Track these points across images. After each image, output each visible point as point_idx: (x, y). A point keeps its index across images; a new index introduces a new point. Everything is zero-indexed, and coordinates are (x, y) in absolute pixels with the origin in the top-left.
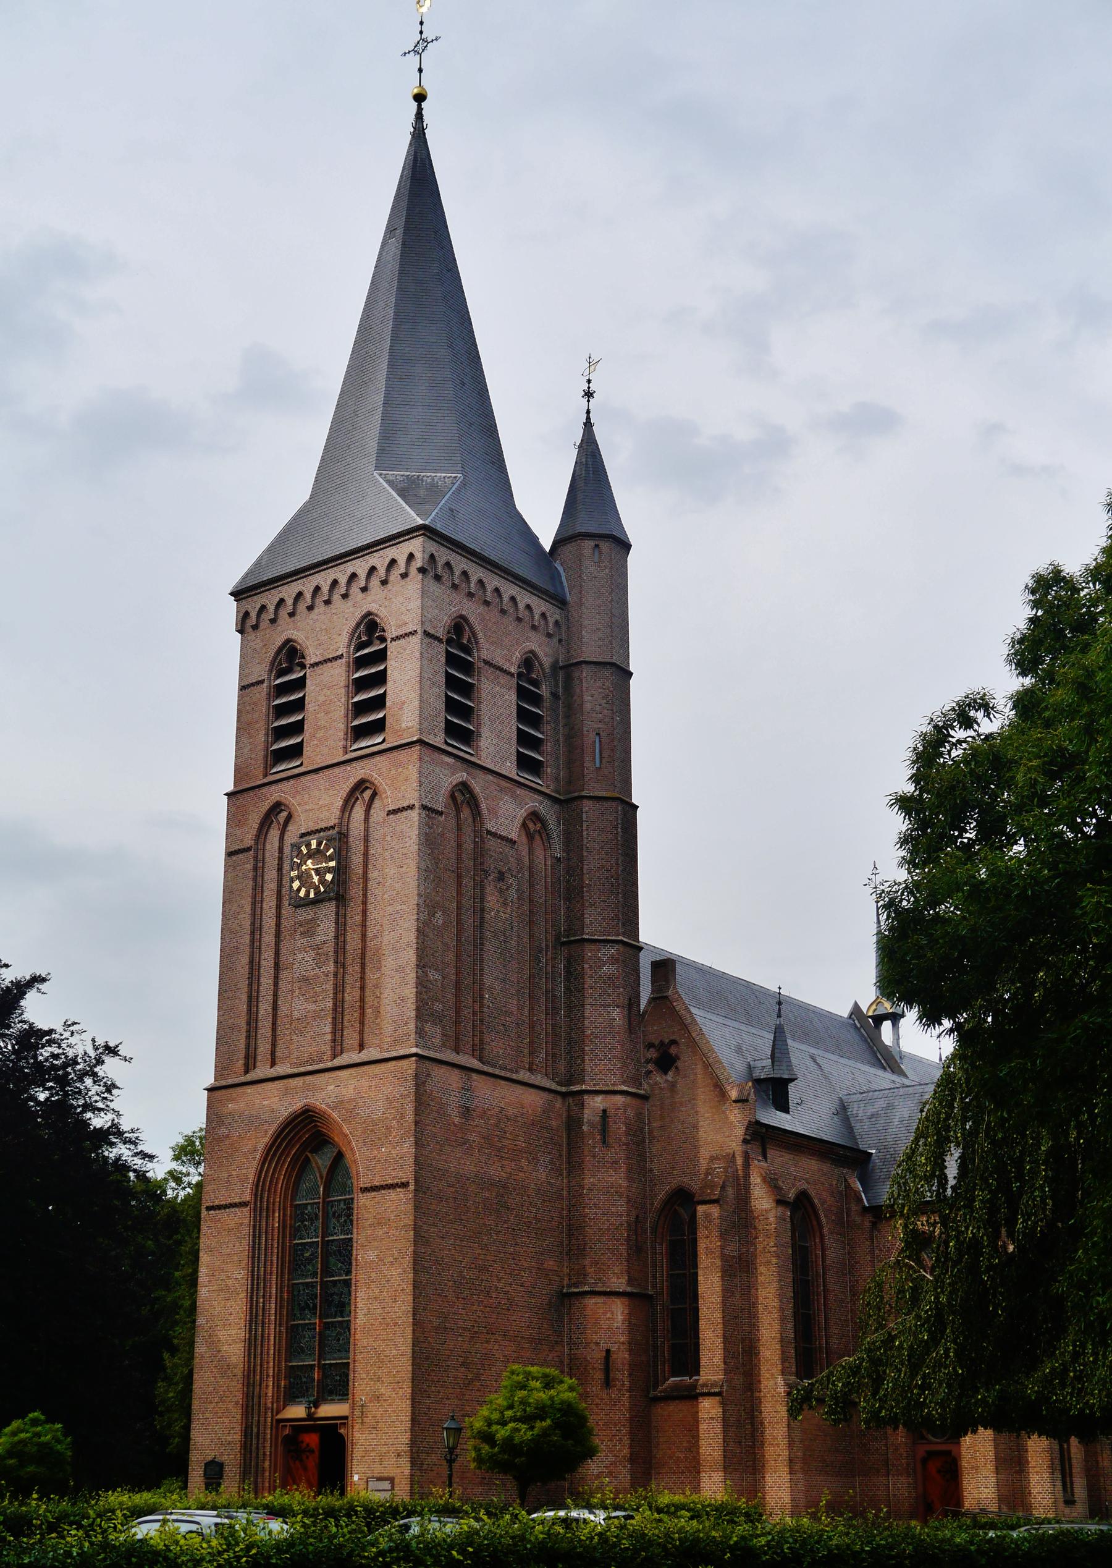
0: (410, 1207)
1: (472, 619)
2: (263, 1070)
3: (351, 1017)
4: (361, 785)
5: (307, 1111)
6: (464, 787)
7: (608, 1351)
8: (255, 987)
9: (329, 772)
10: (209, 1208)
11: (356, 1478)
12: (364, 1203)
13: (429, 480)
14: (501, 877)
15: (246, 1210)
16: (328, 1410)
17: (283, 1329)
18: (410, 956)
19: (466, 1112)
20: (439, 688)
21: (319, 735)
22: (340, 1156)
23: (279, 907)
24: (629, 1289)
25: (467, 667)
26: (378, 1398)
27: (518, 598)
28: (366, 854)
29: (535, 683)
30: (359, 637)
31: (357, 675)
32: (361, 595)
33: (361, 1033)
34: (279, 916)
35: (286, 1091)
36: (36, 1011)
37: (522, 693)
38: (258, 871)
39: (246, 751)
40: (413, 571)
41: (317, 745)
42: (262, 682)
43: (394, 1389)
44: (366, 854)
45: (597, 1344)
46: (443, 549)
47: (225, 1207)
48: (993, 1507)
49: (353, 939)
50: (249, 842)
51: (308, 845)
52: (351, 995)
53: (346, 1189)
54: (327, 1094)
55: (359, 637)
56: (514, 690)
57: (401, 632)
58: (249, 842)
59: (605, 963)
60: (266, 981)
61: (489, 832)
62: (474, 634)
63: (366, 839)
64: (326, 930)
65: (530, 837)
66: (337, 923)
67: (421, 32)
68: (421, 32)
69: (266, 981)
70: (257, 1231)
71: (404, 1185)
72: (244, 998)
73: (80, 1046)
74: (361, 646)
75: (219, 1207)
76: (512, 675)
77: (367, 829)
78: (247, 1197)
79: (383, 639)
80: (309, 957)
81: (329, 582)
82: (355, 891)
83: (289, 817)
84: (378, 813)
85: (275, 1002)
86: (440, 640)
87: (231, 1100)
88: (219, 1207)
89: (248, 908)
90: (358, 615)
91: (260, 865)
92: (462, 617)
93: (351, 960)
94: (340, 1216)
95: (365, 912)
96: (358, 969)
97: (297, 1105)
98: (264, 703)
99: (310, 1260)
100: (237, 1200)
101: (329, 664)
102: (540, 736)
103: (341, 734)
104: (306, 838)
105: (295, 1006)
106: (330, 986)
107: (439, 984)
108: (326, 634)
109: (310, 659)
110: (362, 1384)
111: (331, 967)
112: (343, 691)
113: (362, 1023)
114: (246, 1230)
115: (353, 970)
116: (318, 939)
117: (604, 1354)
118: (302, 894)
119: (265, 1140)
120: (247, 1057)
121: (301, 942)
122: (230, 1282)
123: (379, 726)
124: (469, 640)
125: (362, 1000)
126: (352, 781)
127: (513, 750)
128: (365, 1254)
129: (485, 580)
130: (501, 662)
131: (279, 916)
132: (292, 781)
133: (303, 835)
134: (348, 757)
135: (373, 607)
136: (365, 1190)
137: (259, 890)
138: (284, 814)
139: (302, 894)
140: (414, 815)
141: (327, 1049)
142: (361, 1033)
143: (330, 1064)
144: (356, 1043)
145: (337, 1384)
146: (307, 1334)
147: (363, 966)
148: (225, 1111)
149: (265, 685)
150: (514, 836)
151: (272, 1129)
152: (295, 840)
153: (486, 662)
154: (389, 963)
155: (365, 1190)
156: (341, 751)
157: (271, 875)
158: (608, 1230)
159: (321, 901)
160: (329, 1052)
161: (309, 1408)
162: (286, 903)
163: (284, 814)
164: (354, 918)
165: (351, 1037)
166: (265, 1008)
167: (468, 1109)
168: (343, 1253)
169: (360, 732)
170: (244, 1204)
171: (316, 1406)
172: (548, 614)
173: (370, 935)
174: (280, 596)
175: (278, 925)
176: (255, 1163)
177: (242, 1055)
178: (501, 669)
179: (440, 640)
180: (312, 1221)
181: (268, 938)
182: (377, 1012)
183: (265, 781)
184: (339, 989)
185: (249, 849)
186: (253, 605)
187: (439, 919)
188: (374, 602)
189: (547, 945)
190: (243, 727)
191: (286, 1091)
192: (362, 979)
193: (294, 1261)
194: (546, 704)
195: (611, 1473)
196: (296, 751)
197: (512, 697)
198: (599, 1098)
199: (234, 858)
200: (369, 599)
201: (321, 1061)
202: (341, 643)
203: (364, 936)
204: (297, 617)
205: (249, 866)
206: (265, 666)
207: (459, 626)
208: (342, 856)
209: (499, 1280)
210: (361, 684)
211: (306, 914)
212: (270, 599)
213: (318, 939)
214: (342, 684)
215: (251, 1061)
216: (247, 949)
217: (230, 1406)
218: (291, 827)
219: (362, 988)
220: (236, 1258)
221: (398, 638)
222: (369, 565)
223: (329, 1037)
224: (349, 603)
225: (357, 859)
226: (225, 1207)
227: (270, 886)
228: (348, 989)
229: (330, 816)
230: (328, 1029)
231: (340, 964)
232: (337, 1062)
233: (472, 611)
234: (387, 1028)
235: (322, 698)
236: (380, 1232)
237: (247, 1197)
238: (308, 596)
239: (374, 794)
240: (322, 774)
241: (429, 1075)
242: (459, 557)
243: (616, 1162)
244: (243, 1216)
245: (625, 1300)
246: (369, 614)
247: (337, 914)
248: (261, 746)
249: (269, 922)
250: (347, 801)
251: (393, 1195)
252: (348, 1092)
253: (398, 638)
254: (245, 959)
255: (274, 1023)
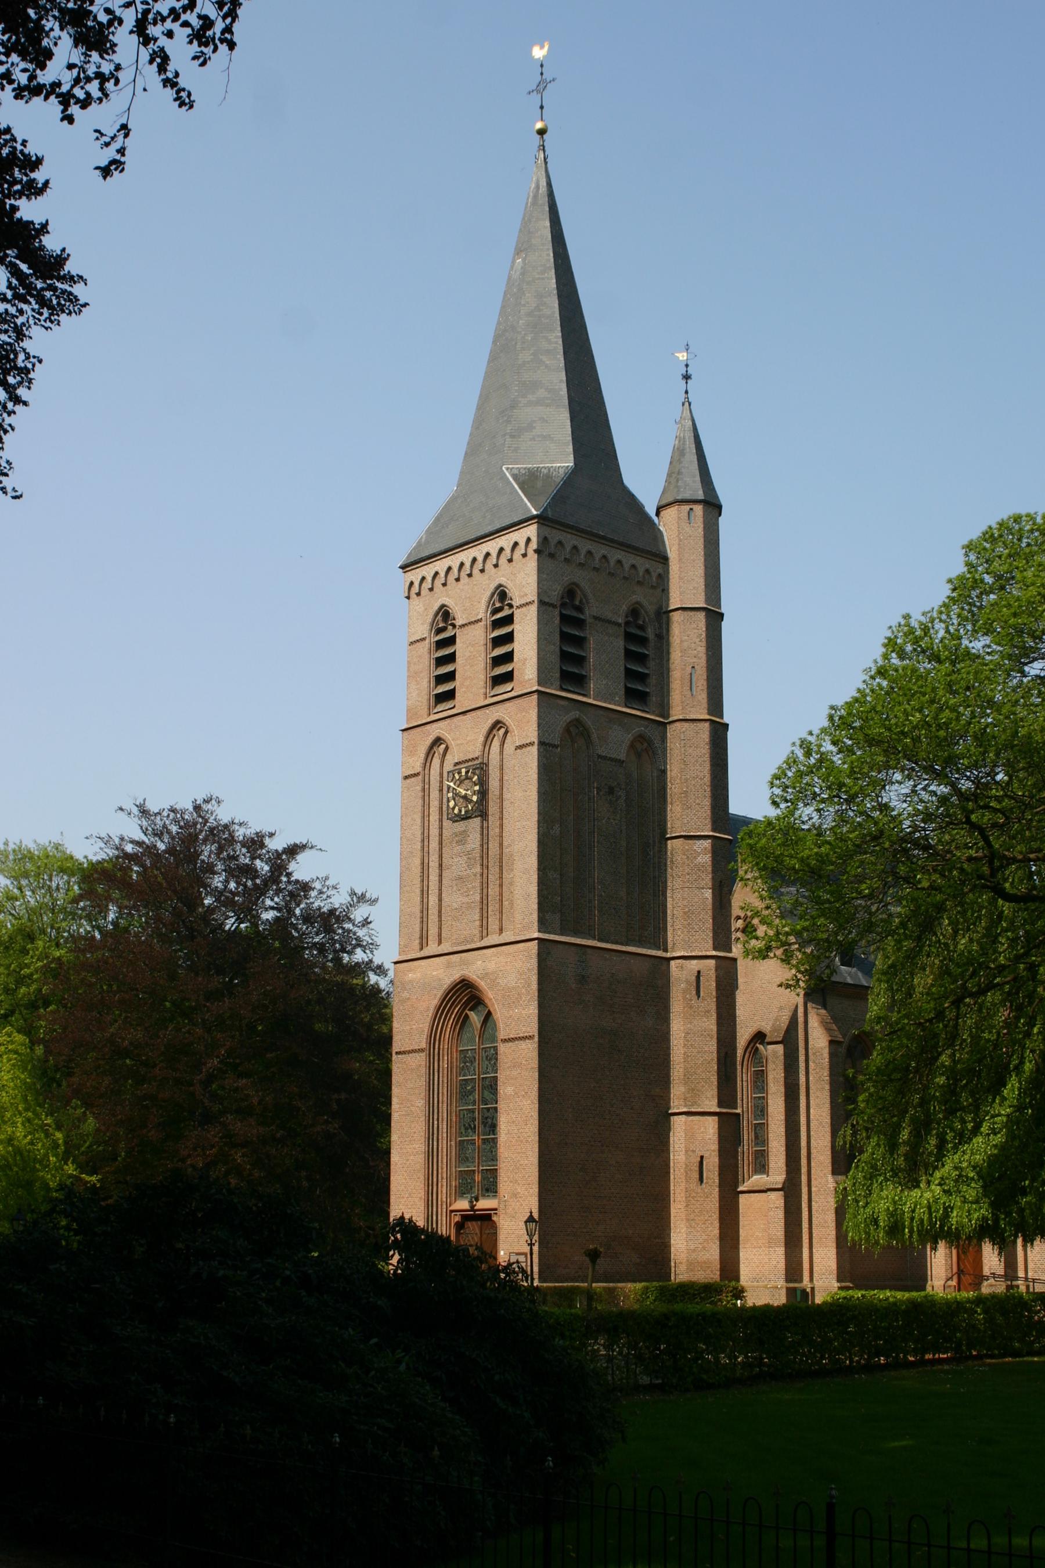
0: (535, 1054)
1: (582, 584)
2: (432, 948)
3: (493, 907)
4: (497, 724)
5: (463, 980)
6: (577, 723)
7: (702, 1157)
8: (425, 883)
9: (473, 714)
10: (397, 1053)
11: (502, 1253)
12: (504, 1050)
13: (546, 471)
14: (611, 791)
15: (423, 1055)
16: (483, 1204)
17: (453, 1143)
18: (533, 861)
19: (583, 979)
20: (554, 644)
21: (467, 683)
22: (489, 1014)
23: (441, 820)
24: (718, 1110)
25: (580, 623)
26: (515, 1195)
27: (624, 561)
28: (501, 780)
29: (642, 628)
30: (494, 604)
31: (493, 635)
32: (494, 570)
33: (501, 920)
34: (441, 828)
35: (449, 965)
36: (301, 869)
37: (629, 637)
38: (425, 792)
39: (414, 695)
40: (530, 552)
41: (465, 692)
42: (424, 639)
43: (526, 1189)
44: (501, 780)
45: (694, 1151)
46: (555, 531)
47: (410, 1052)
48: (718, 1280)
49: (493, 846)
50: (418, 768)
51: (459, 773)
52: (493, 891)
53: (494, 1039)
54: (477, 968)
55: (494, 604)
56: (622, 637)
57: (523, 601)
58: (418, 768)
59: (699, 854)
60: (434, 878)
61: (599, 756)
62: (585, 596)
63: (502, 768)
64: (474, 841)
65: (639, 755)
66: (482, 834)
67: (542, 74)
68: (542, 74)
69: (434, 878)
70: (431, 1071)
71: (531, 1037)
72: (418, 891)
73: (339, 900)
74: (496, 611)
75: (404, 1053)
76: (619, 625)
77: (502, 760)
78: (423, 1045)
79: (511, 606)
80: (463, 861)
81: (470, 559)
82: (493, 808)
83: (447, 749)
84: (509, 747)
85: (440, 895)
86: (554, 606)
87: (410, 971)
88: (404, 1053)
89: (419, 821)
90: (493, 586)
91: (427, 786)
92: (574, 584)
93: (490, 862)
94: (490, 1059)
95: (501, 826)
96: (497, 870)
97: (456, 976)
98: (427, 656)
99: (472, 1092)
100: (417, 1048)
101: (473, 626)
102: (646, 671)
103: (482, 683)
104: (458, 767)
105: (453, 899)
106: (477, 884)
107: (558, 882)
108: (470, 602)
109: (459, 622)
110: (504, 1185)
111: (478, 869)
112: (483, 648)
113: (501, 912)
114: (423, 1070)
115: (494, 870)
116: (469, 847)
117: (699, 1159)
118: (456, 811)
119: (435, 1002)
120: (421, 938)
121: (458, 849)
122: (413, 1109)
123: (508, 677)
124: (581, 601)
125: (501, 894)
126: (490, 722)
127: (622, 686)
128: (505, 1090)
129: (593, 551)
130: (609, 615)
131: (441, 828)
132: (448, 721)
133: (456, 764)
134: (487, 702)
135: (503, 580)
136: (505, 1041)
137: (426, 807)
138: (443, 746)
139: (456, 811)
140: (534, 750)
141: (477, 932)
142: (501, 920)
143: (479, 945)
144: (497, 928)
145: (491, 1188)
146: (470, 1147)
147: (501, 867)
148: (407, 979)
149: (427, 641)
150: (622, 756)
151: (440, 994)
152: (451, 768)
153: (596, 618)
154: (518, 865)
155: (505, 1041)
156: (482, 696)
157: (435, 794)
158: (702, 1064)
159: (470, 818)
160: (478, 935)
161: (471, 1202)
162: (445, 817)
163: (443, 746)
164: (494, 831)
165: (494, 925)
166: (433, 900)
167: (583, 977)
168: (492, 1086)
169: (498, 680)
170: (422, 1050)
171: (477, 1200)
172: (651, 570)
173: (505, 844)
174: (436, 569)
175: (441, 835)
176: (429, 1019)
177: (418, 935)
178: (609, 622)
179: (554, 606)
180: (472, 1062)
181: (434, 844)
182: (512, 904)
183: (429, 720)
184: (484, 886)
185: (418, 774)
186: (415, 576)
187: (557, 829)
188: (502, 576)
189: (654, 841)
190: (412, 676)
191: (449, 965)
192: (501, 878)
193: (463, 1092)
194: (652, 644)
195: (704, 1248)
196: (450, 695)
197: (620, 643)
198: (694, 962)
199: (408, 781)
200: (500, 573)
201: (473, 941)
202: (481, 610)
203: (501, 845)
204: (448, 587)
205: (419, 788)
206: (427, 627)
207: (570, 592)
208: (483, 782)
209: (612, 1106)
210: (497, 642)
211: (461, 826)
212: (427, 571)
213: (469, 847)
214: (482, 642)
215: (424, 941)
216: (419, 854)
217: (416, 1200)
218: (448, 757)
219: (501, 886)
220: (417, 1091)
221: (521, 606)
222: (499, 546)
223: (478, 923)
224: (486, 575)
225: (493, 784)
226: (410, 1052)
227: (435, 804)
228: (491, 886)
229: (474, 750)
230: (477, 917)
231: (485, 866)
232: (486, 942)
233: (582, 578)
234: (518, 917)
235: (468, 654)
236: (515, 1073)
237: (423, 1045)
238: (455, 570)
239: (506, 732)
240: (469, 716)
241: (549, 953)
242: (569, 536)
243: (708, 1011)
244: (421, 1059)
245: (716, 1118)
246: (500, 586)
247: (482, 827)
248: (425, 692)
249: (434, 831)
250: (487, 738)
251: (523, 1045)
252: (491, 966)
253: (521, 606)
254: (417, 861)
255: (440, 911)
